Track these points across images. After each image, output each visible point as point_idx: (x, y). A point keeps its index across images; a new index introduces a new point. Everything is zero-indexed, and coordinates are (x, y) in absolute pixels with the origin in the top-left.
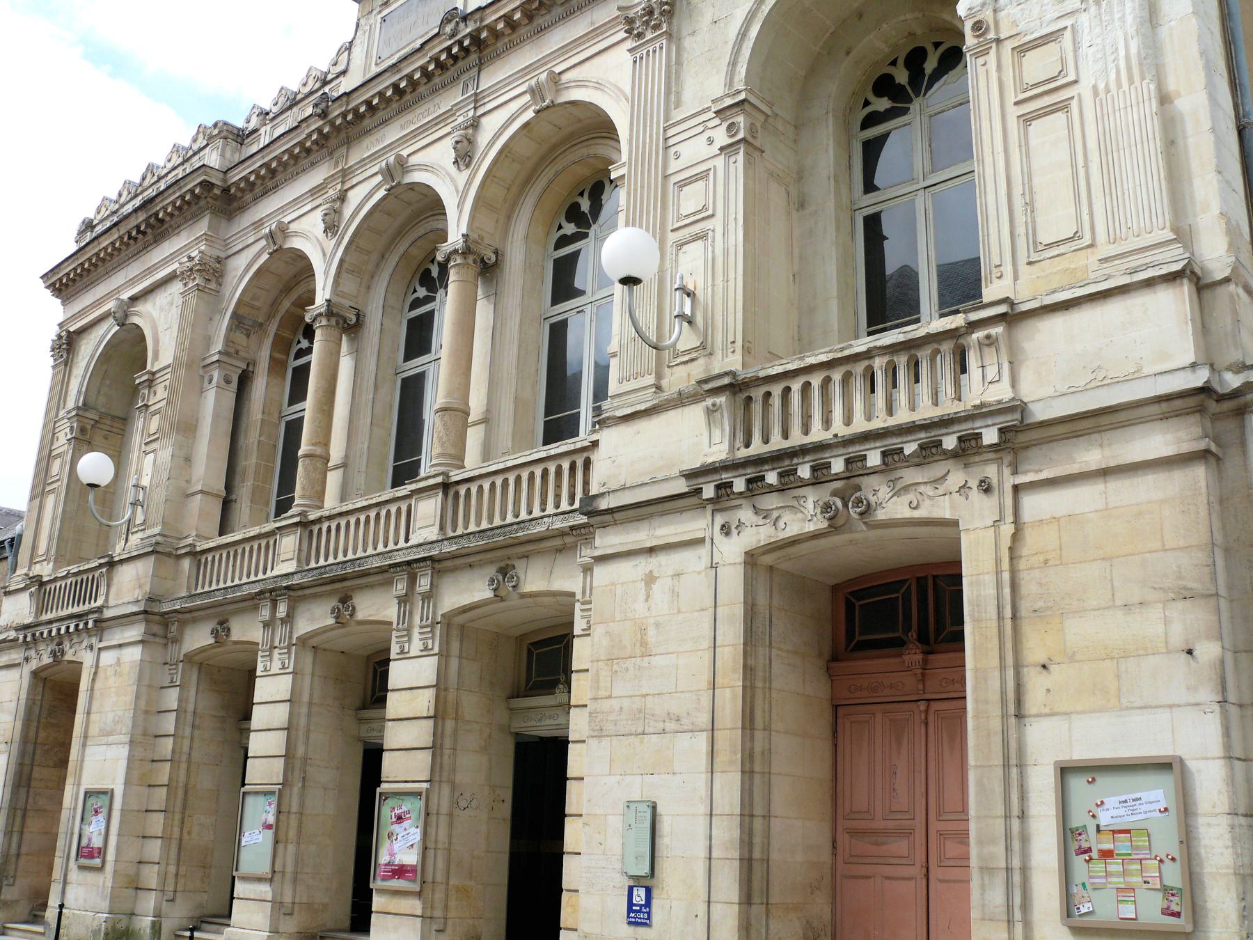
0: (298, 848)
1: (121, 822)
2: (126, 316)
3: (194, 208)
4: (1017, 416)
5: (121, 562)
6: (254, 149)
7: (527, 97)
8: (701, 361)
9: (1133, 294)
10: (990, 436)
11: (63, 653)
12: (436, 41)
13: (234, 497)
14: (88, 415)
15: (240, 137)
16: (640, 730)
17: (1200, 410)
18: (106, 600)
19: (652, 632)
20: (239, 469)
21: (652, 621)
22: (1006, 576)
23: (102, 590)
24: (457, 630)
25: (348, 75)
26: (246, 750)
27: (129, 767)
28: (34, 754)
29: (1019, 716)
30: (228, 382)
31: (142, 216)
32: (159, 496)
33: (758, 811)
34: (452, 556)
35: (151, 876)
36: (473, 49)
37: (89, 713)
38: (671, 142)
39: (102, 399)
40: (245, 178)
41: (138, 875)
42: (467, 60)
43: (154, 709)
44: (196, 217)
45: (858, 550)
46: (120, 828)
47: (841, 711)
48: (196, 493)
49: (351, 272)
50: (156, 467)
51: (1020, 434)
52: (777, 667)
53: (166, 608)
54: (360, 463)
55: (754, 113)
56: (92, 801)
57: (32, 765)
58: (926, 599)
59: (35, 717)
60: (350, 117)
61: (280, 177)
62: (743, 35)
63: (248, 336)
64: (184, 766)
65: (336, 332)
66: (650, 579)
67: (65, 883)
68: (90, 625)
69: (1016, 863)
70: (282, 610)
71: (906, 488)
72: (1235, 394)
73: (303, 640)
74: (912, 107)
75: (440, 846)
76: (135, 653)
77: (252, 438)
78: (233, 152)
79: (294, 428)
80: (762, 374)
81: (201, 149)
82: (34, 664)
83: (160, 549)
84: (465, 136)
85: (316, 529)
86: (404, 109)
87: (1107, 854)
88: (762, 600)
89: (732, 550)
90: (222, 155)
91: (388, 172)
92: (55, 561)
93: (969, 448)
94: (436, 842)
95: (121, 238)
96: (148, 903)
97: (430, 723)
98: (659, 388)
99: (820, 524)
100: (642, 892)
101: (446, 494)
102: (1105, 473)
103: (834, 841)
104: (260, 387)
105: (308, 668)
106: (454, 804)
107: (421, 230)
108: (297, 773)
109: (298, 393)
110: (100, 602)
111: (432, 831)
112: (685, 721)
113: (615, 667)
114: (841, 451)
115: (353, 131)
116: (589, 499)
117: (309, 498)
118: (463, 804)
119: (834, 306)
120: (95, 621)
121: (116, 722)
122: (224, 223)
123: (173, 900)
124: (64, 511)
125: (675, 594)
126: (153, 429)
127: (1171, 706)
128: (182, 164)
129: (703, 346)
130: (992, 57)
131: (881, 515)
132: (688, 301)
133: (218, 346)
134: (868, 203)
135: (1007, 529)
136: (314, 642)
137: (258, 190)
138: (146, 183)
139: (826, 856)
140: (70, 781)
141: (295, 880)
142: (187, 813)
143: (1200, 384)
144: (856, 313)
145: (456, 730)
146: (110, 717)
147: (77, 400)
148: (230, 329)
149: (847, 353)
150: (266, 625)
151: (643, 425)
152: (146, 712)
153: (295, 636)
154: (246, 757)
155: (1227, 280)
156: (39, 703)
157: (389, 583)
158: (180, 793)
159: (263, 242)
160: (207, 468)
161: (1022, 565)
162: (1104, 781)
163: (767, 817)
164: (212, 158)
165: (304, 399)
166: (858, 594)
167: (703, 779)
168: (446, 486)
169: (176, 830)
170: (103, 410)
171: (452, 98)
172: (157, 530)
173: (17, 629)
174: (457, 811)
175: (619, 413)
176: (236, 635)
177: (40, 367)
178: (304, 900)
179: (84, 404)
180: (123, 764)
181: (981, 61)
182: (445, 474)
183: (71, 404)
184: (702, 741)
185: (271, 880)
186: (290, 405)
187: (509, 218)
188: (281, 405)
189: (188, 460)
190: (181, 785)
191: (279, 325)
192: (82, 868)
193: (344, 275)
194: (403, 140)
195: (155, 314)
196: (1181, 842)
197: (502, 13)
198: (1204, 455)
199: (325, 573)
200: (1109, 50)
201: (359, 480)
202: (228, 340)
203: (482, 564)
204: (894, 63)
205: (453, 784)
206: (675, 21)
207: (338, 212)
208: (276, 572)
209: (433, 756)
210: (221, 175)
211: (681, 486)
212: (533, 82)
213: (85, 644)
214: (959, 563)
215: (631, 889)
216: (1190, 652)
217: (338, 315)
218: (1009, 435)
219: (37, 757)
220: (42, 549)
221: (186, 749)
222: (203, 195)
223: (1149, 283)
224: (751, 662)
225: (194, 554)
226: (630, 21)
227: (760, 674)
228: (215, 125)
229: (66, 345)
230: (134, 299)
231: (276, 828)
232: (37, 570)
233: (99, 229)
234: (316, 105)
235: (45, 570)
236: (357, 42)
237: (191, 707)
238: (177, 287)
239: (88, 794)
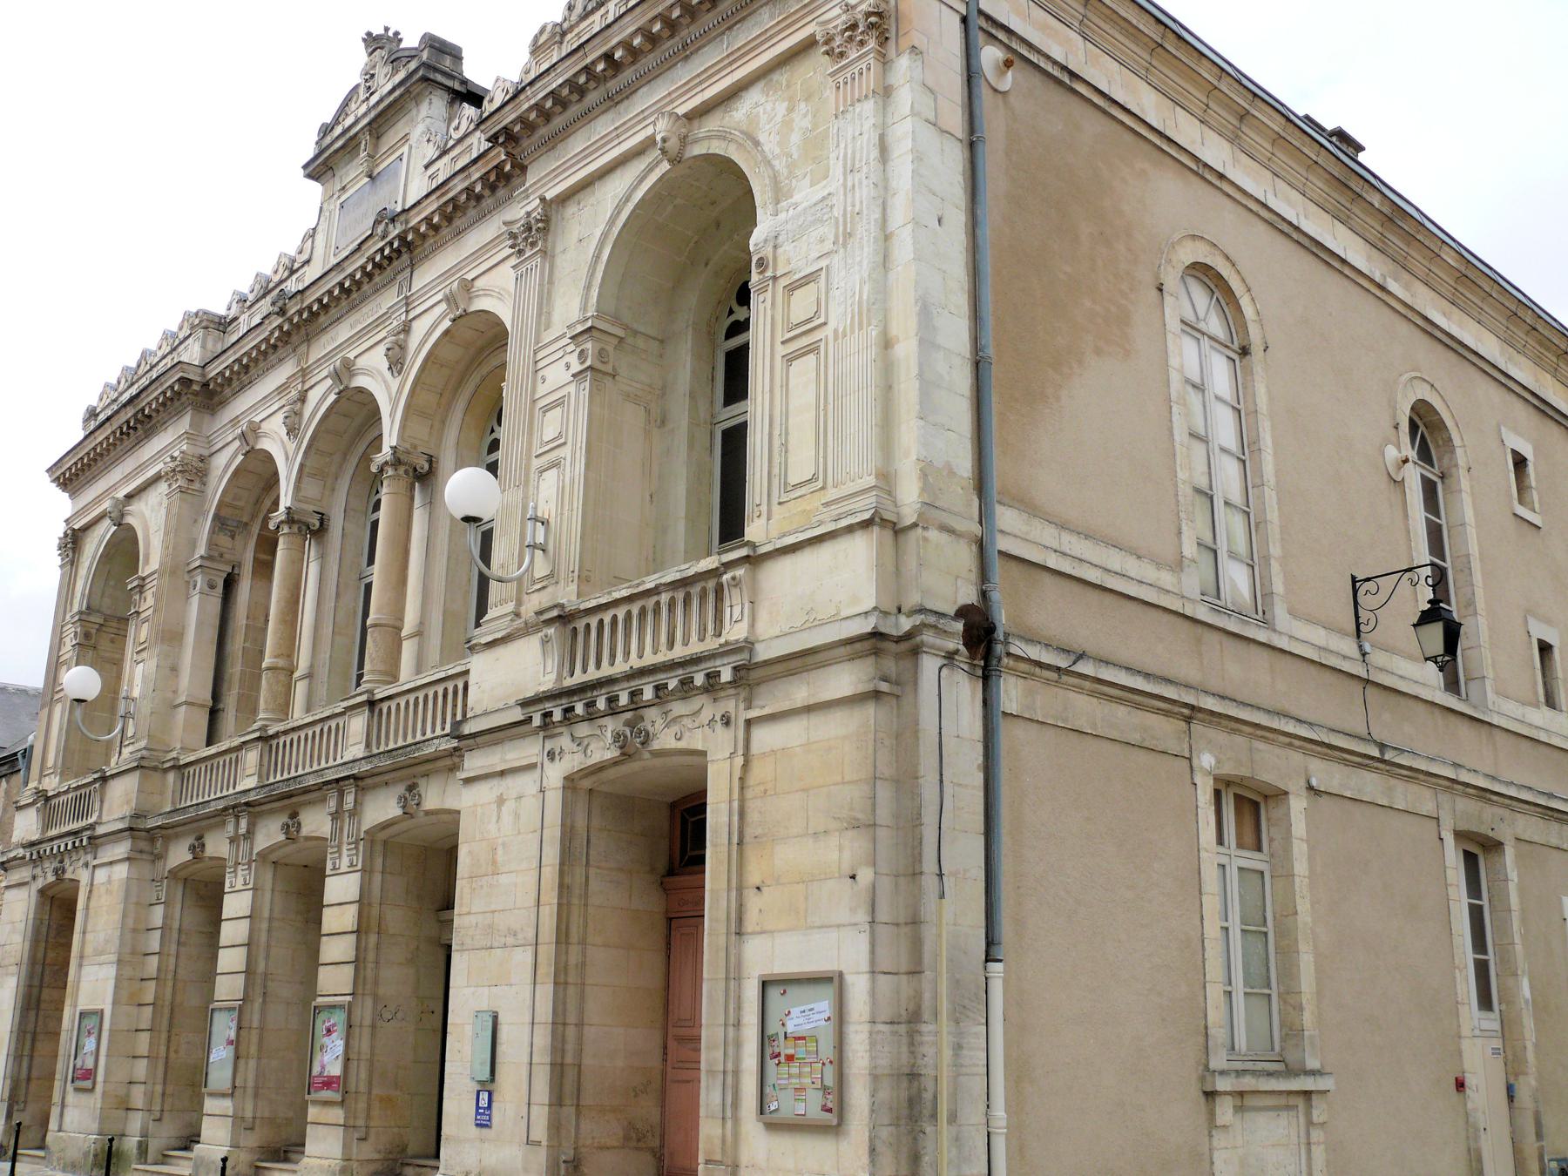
0: (258, 1065)
1: (110, 1041)
2: (122, 515)
3: (177, 403)
4: (745, 655)
5: (113, 776)
6: (234, 338)
7: (443, 306)
8: (550, 589)
9: (840, 540)
10: (726, 675)
11: (64, 871)
12: (370, 242)
13: (221, 706)
14: (92, 619)
15: (222, 325)
17: (876, 652)
18: (100, 816)
19: (500, 852)
20: (226, 677)
22: (736, 804)
23: (97, 806)
24: (381, 842)
29: (739, 934)
30: (212, 587)
31: (130, 412)
32: (146, 708)
33: (572, 1018)
34: (372, 774)
35: (138, 1096)
36: (404, 250)
38: (540, 365)
39: (107, 601)
40: (221, 373)
41: (128, 1095)
43: (143, 926)
44: (179, 413)
48: (180, 705)
49: (311, 475)
50: (158, 674)
51: (751, 674)
52: (594, 886)
53: (151, 824)
54: (323, 673)
55: (604, 337)
56: (86, 1022)
57: (41, 987)
59: (580, 840)
60: (305, 315)
61: (253, 371)
62: (597, 257)
63: (233, 537)
64: (170, 984)
65: (299, 540)
66: (501, 801)
67: (63, 1106)
69: (730, 1067)
70: (243, 823)
71: (674, 720)
72: (908, 636)
73: (262, 855)
75: (363, 1057)
76: (122, 871)
78: (215, 342)
80: (582, 607)
81: (186, 338)
82: (40, 883)
83: (144, 763)
84: (396, 343)
85: (274, 742)
86: (353, 308)
87: (790, 1058)
88: (581, 822)
89: (555, 774)
90: (203, 347)
91: (336, 376)
92: (62, 774)
93: (712, 685)
95: (114, 432)
96: (135, 1123)
98: (517, 615)
99: (612, 753)
101: (372, 711)
102: (809, 709)
103: (665, 1048)
105: (268, 885)
106: (378, 1015)
107: (485, 370)
108: (258, 990)
111: (355, 1043)
112: (520, 936)
114: (626, 685)
115: (311, 328)
116: (457, 725)
117: (273, 711)
118: (387, 1015)
119: (681, 527)
121: (107, 941)
122: (207, 418)
123: (159, 1120)
125: (517, 816)
127: (838, 926)
128: (170, 352)
129: (551, 575)
130: (769, 294)
131: (656, 745)
132: (540, 529)
133: (202, 550)
134: (728, 416)
135: (739, 761)
136: (273, 857)
137: (235, 384)
138: (140, 372)
139: (655, 1062)
140: (68, 1002)
141: (256, 1095)
142: (174, 1031)
143: (869, 629)
144: (710, 529)
146: (102, 936)
147: (81, 604)
148: (212, 532)
149: (641, 589)
150: (232, 840)
151: (501, 652)
152: (134, 930)
153: (255, 851)
155: (915, 525)
157: (324, 800)
158: (167, 1011)
159: (237, 443)
160: (193, 679)
161: (749, 794)
162: (794, 992)
163: (580, 1025)
164: (192, 353)
167: (529, 988)
168: (372, 704)
169: (163, 1049)
171: (389, 299)
172: (143, 744)
173: (24, 847)
174: (379, 1024)
175: (483, 641)
176: (210, 850)
177: (48, 570)
178: (267, 1114)
179: (88, 608)
180: (111, 984)
181: (761, 298)
182: (370, 692)
183: (76, 609)
185: (232, 1095)
187: (443, 422)
189: (174, 670)
191: (248, 530)
192: (77, 1090)
193: (305, 479)
194: (349, 342)
195: (147, 513)
197: (423, 216)
198: (876, 695)
200: (849, 294)
201: (322, 691)
202: (211, 544)
203: (395, 782)
205: (376, 999)
206: (550, 239)
207: (299, 414)
208: (239, 788)
209: (357, 969)
210: (199, 370)
211: (517, 715)
212: (447, 290)
213: (706, 715)
214: (704, 793)
216: (853, 877)
217: (299, 522)
218: (743, 673)
219: (46, 979)
220: (50, 763)
221: (172, 967)
222: (172, 396)
223: (850, 529)
224: (567, 880)
225: (179, 768)
226: (513, 236)
227: (577, 892)
229: (73, 542)
230: (130, 497)
231: (236, 1043)
233: (102, 417)
234: (273, 304)
235: (51, 784)
236: (320, 228)
237: (176, 925)
238: (163, 487)
239: (83, 1015)
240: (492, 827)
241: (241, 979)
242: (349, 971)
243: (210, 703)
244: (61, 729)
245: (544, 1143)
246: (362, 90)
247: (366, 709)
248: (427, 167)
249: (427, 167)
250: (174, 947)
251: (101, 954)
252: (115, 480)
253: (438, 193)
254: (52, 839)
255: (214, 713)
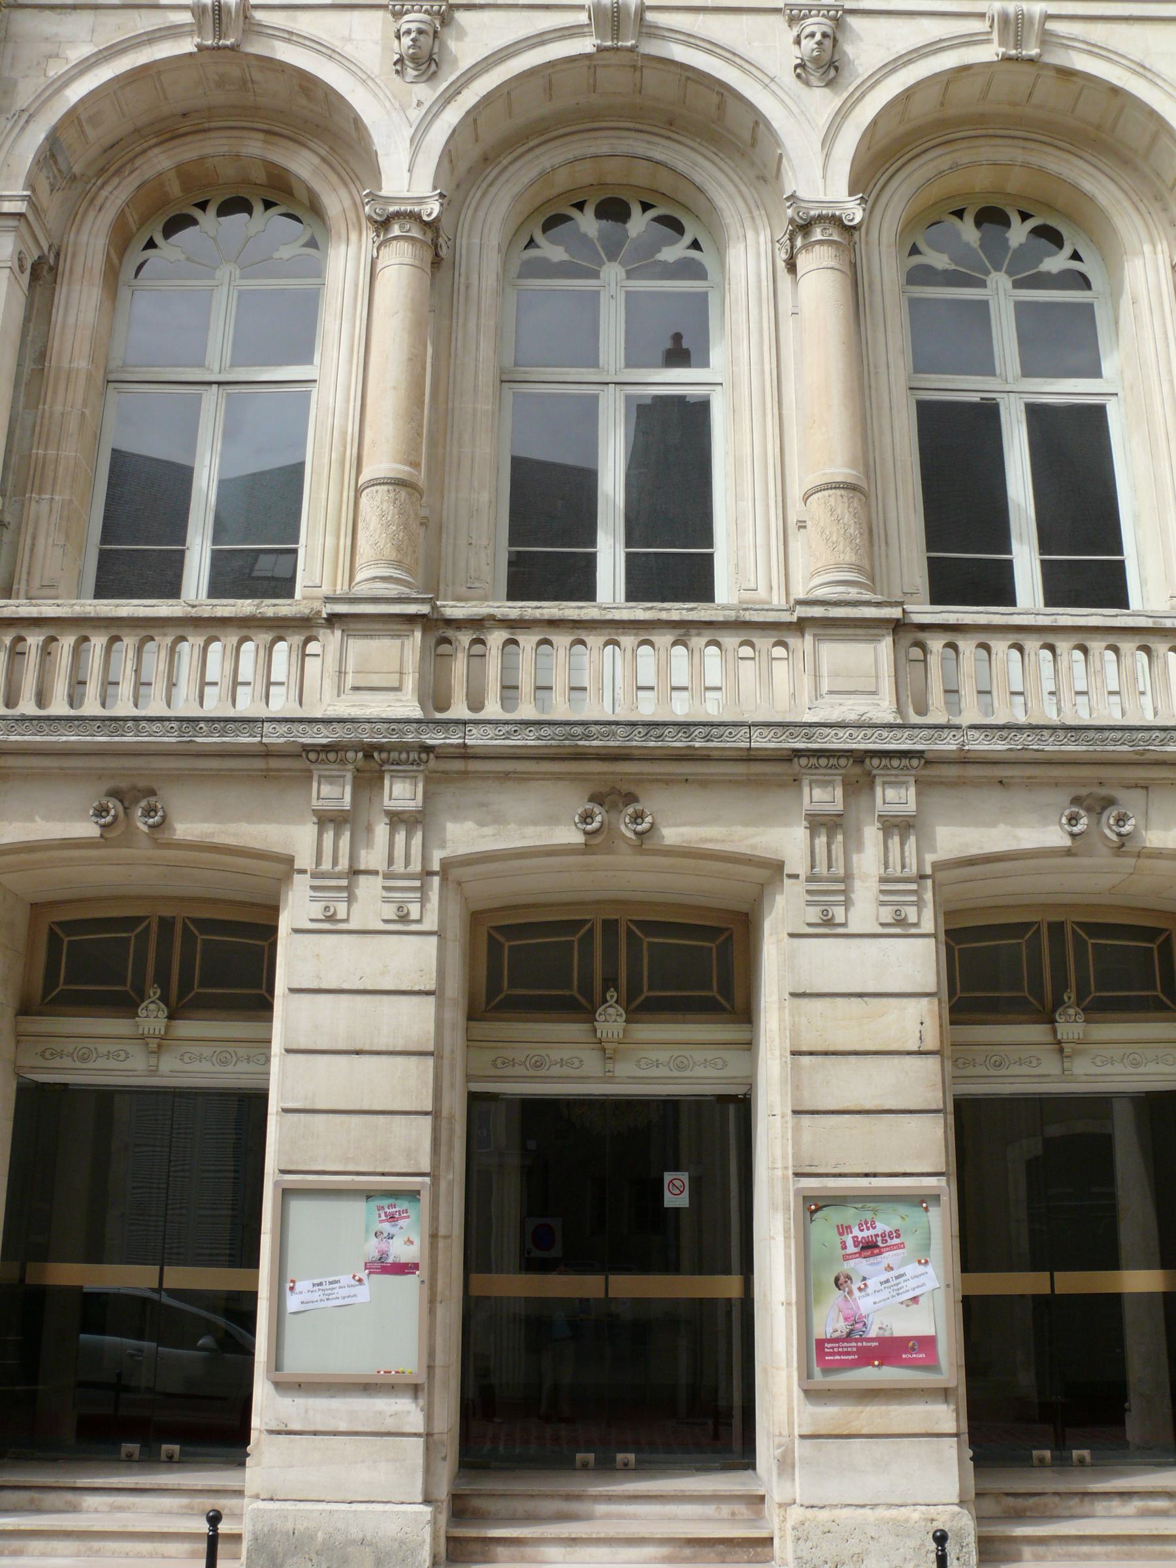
45: (130, 873)
58: (954, 963)
97: (932, 1064)
166: (510, 931)
196: (948, 1286)
199: (587, 737)
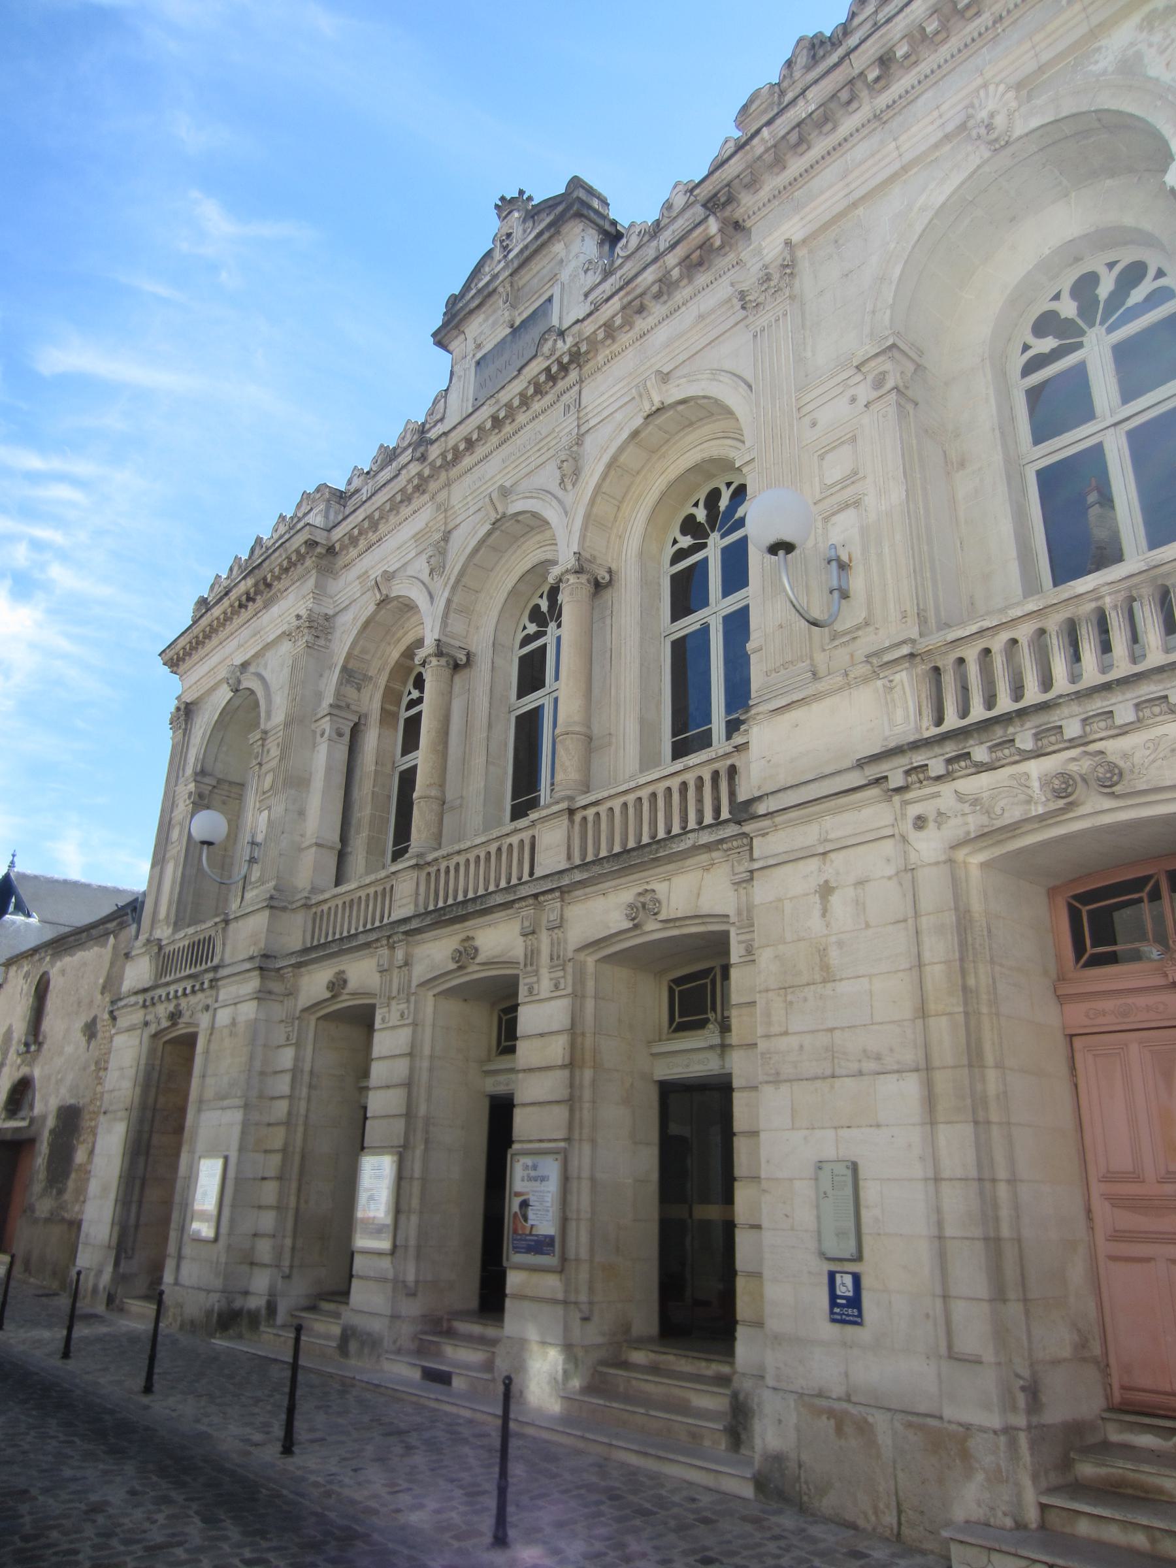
15: (341, 497)
16: (828, 1072)
19: (834, 954)
20: (354, 822)
21: (833, 939)
25: (445, 421)
26: (365, 1108)
27: (243, 1133)
28: (153, 1121)
30: (340, 735)
37: (204, 1076)
38: (804, 411)
41: (253, 1248)
42: (567, 379)
46: (234, 1199)
47: (1078, 1042)
57: (151, 1132)
63: (359, 690)
64: (301, 1129)
66: (826, 890)
67: (180, 1258)
68: (206, 985)
74: (1085, 339)
77: (365, 789)
78: (336, 513)
79: (408, 779)
83: (275, 903)
94: (578, 1211)
100: (848, 1280)
101: (572, 821)
103: (1089, 1211)
104: (371, 740)
109: (411, 742)
110: (216, 961)
113: (789, 998)
120: (211, 981)
124: (183, 875)
125: (859, 905)
126: (267, 785)
133: (329, 699)
141: (418, 1257)
145: (594, 1082)
147: (195, 765)
148: (340, 683)
154: (365, 1118)
156: (158, 1068)
158: (297, 1158)
160: (318, 815)
165: (417, 748)
169: (293, 1199)
170: (221, 776)
180: (236, 1131)
182: (571, 799)
184: (911, 1086)
186: (403, 755)
188: (394, 756)
190: (298, 1150)
202: (338, 694)
204: (1057, 297)
208: (394, 918)
215: (832, 1276)
217: (448, 655)
221: (303, 1111)
228: (318, 490)
229: (186, 713)
232: (158, 934)
235: (163, 932)
237: (307, 1067)
240: (815, 923)
241: (400, 1125)
242: (560, 1114)
243: (339, 846)
244: (174, 882)
245: (989, 1356)
246: (498, 255)
247: (566, 817)
248: (586, 295)
249: (586, 295)
250: (305, 1091)
251: (223, 1098)
252: (231, 650)
253: (622, 293)
254: (167, 984)
255: (342, 857)
